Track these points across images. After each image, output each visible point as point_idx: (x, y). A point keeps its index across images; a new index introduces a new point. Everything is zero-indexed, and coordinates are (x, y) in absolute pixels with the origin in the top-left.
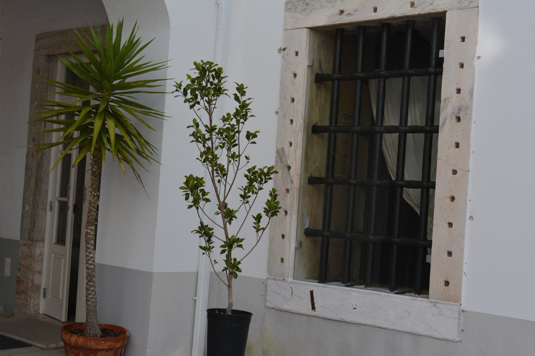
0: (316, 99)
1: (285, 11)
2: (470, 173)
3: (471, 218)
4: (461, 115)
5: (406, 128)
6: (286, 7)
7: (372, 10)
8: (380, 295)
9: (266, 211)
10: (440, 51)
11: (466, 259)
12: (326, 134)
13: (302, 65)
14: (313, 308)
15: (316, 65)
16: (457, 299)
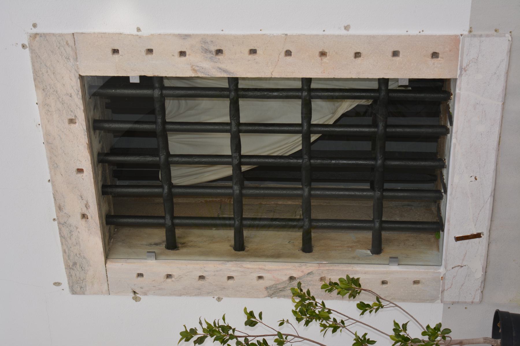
0: (199, 247)
1: (84, 294)
2: (289, 33)
3: (347, 28)
4: (214, 48)
5: (233, 123)
6: (79, 294)
7: (80, 175)
8: (455, 145)
9: (353, 295)
10: (131, 81)
11: (402, 32)
12: (246, 233)
13: (156, 267)
14: (478, 236)
15: (156, 249)
16: (456, 40)
